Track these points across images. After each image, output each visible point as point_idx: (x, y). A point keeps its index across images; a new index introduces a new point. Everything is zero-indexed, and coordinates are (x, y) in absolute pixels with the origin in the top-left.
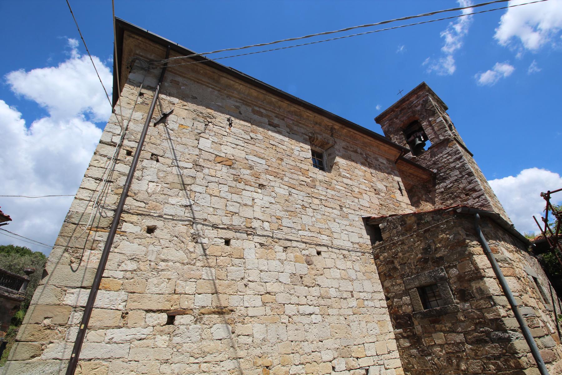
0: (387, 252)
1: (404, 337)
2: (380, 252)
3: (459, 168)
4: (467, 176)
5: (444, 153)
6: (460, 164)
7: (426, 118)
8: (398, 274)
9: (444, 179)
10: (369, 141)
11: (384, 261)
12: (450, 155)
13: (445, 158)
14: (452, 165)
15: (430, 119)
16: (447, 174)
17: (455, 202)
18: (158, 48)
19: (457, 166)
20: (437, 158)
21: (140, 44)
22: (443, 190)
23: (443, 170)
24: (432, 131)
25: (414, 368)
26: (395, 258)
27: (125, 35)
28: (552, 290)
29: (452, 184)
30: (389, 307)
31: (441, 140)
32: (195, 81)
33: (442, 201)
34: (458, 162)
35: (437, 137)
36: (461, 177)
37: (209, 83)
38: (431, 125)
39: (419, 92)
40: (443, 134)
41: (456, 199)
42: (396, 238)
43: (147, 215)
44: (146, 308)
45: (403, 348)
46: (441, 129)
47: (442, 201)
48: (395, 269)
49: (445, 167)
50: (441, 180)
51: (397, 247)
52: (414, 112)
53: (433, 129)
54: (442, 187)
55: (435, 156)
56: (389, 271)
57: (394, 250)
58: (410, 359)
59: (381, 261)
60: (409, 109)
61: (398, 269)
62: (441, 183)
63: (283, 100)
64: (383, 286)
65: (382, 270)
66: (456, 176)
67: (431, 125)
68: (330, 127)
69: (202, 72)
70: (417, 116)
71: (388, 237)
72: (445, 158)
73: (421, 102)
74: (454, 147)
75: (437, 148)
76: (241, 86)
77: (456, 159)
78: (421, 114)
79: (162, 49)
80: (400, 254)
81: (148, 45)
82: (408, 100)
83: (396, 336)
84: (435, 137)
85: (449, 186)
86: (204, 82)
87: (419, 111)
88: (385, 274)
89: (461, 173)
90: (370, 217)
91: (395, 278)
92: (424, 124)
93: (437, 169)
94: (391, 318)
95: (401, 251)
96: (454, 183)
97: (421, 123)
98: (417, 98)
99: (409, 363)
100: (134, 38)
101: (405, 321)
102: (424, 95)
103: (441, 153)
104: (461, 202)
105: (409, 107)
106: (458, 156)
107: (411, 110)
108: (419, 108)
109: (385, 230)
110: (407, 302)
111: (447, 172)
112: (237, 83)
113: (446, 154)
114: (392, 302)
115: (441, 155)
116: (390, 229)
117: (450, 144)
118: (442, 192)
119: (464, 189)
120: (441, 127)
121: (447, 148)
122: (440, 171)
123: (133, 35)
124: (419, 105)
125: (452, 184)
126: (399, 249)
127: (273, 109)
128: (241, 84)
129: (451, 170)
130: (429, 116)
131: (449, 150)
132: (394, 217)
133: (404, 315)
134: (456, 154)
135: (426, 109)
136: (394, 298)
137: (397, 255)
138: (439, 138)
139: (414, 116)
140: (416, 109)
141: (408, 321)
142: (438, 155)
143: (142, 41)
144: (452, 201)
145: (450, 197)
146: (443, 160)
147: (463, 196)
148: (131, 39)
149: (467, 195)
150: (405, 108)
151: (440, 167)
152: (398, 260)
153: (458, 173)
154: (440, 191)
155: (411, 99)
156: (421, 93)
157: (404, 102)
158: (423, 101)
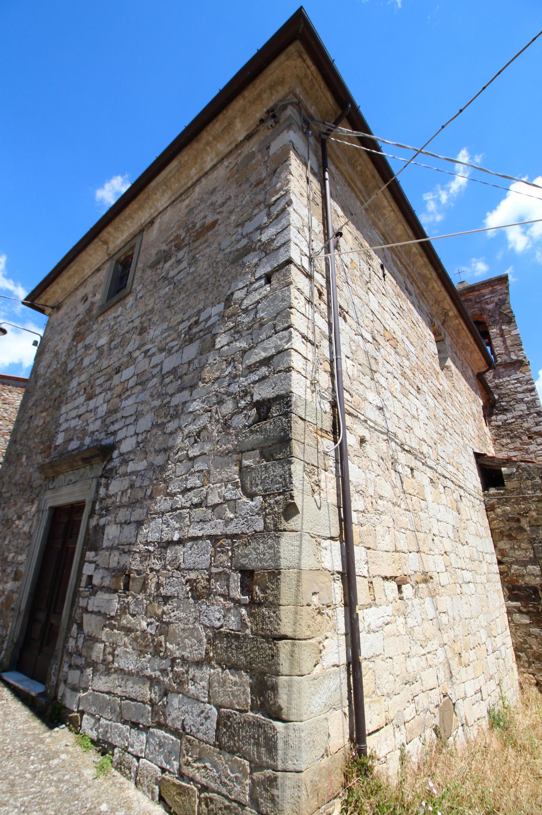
0: (510, 506)
1: (520, 612)
2: (498, 504)
3: (527, 403)
4: (535, 415)
5: (513, 377)
6: (530, 398)
7: (498, 324)
8: (525, 537)
9: (504, 411)
10: (469, 343)
11: (502, 516)
12: (520, 382)
13: (513, 384)
14: (520, 396)
15: (503, 327)
16: (511, 406)
17: (513, 442)
18: (327, 99)
19: (526, 399)
20: (501, 380)
21: (307, 77)
22: (500, 423)
23: (507, 399)
24: (502, 343)
25: (532, 648)
26: (523, 516)
27: (292, 49)
28: (301, 504)
29: (514, 420)
30: (501, 573)
31: (512, 359)
32: (346, 181)
33: (495, 438)
34: (528, 394)
35: (508, 354)
36: (527, 415)
37: (361, 192)
38: (502, 336)
39: (496, 285)
40: (517, 352)
41: (515, 439)
42: (529, 492)
43: (355, 416)
44: (383, 575)
45: (517, 625)
46: (516, 345)
47: (495, 438)
48: (521, 529)
49: (509, 396)
50: (501, 410)
51: (529, 503)
52: (482, 310)
53: (504, 341)
54: (500, 420)
55: (499, 378)
56: (510, 529)
57: (523, 506)
58: (528, 639)
59: (497, 515)
60: (477, 303)
61: (526, 531)
62: (500, 414)
63: (424, 255)
64: (495, 546)
65: (497, 526)
66: (522, 411)
67: (502, 336)
68: (446, 311)
69: (359, 168)
70: (485, 316)
71: (515, 487)
72: (513, 384)
73: (496, 299)
74: (527, 374)
75: (503, 367)
76: (392, 214)
77: (526, 390)
78: (492, 316)
79: (332, 103)
80: (534, 513)
81: (317, 87)
82: (478, 290)
83: (507, 610)
84: (505, 354)
85: (510, 421)
86: (357, 187)
87: (489, 311)
88: (501, 532)
89: (528, 409)
90: (485, 454)
91: (521, 541)
92: (493, 331)
93: (499, 395)
94: (503, 588)
95: (535, 510)
96: (516, 419)
97: (490, 328)
98: (492, 292)
99: (525, 642)
100: (304, 61)
101: (527, 594)
102: (503, 292)
103: (509, 376)
104: (521, 444)
105: (478, 300)
106: (529, 387)
107: (479, 305)
108: (491, 307)
109: (512, 477)
110: (534, 572)
111: (511, 403)
112: (391, 206)
113: (514, 379)
114: (509, 569)
115: (508, 379)
116: (521, 478)
117: (522, 369)
118: (499, 427)
119: (528, 429)
120: (516, 342)
121: (518, 373)
122: (502, 398)
123: (306, 56)
124: (492, 302)
125: (514, 420)
126: (533, 507)
127: (408, 264)
128: (393, 211)
129: (517, 402)
130: (503, 323)
131: (519, 375)
132: (530, 465)
133: (526, 587)
134: (527, 384)
135: (500, 312)
136: (512, 563)
137: (527, 513)
138: (510, 357)
139: (481, 315)
140: (487, 306)
141: (532, 595)
142: (504, 377)
143: (312, 75)
144: (509, 441)
145: (508, 434)
146: (510, 387)
147: (525, 438)
148: (299, 62)
149: (530, 438)
150: (470, 300)
151: (504, 394)
152: (528, 519)
153: (525, 408)
154: (496, 423)
155: (483, 291)
156: (498, 287)
157: (473, 291)
158: (499, 299)
